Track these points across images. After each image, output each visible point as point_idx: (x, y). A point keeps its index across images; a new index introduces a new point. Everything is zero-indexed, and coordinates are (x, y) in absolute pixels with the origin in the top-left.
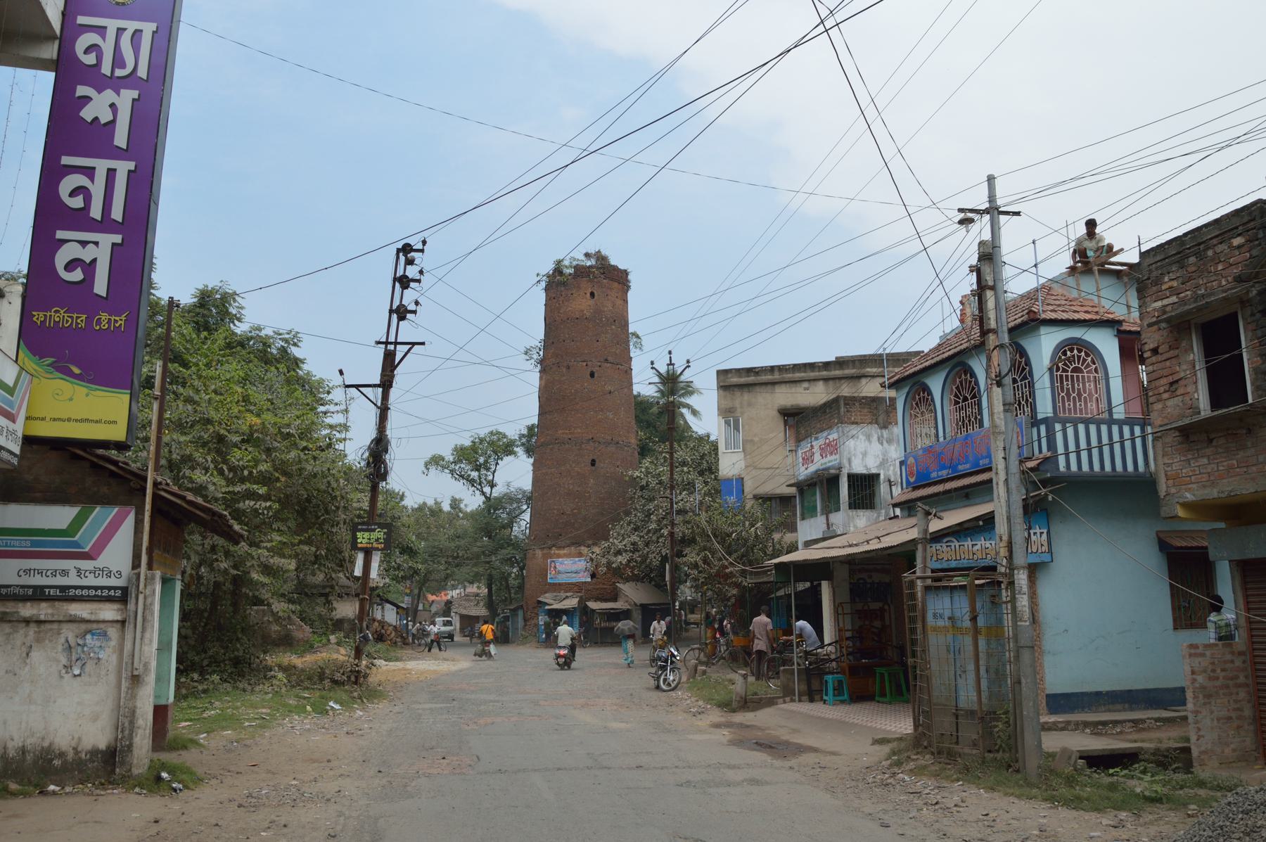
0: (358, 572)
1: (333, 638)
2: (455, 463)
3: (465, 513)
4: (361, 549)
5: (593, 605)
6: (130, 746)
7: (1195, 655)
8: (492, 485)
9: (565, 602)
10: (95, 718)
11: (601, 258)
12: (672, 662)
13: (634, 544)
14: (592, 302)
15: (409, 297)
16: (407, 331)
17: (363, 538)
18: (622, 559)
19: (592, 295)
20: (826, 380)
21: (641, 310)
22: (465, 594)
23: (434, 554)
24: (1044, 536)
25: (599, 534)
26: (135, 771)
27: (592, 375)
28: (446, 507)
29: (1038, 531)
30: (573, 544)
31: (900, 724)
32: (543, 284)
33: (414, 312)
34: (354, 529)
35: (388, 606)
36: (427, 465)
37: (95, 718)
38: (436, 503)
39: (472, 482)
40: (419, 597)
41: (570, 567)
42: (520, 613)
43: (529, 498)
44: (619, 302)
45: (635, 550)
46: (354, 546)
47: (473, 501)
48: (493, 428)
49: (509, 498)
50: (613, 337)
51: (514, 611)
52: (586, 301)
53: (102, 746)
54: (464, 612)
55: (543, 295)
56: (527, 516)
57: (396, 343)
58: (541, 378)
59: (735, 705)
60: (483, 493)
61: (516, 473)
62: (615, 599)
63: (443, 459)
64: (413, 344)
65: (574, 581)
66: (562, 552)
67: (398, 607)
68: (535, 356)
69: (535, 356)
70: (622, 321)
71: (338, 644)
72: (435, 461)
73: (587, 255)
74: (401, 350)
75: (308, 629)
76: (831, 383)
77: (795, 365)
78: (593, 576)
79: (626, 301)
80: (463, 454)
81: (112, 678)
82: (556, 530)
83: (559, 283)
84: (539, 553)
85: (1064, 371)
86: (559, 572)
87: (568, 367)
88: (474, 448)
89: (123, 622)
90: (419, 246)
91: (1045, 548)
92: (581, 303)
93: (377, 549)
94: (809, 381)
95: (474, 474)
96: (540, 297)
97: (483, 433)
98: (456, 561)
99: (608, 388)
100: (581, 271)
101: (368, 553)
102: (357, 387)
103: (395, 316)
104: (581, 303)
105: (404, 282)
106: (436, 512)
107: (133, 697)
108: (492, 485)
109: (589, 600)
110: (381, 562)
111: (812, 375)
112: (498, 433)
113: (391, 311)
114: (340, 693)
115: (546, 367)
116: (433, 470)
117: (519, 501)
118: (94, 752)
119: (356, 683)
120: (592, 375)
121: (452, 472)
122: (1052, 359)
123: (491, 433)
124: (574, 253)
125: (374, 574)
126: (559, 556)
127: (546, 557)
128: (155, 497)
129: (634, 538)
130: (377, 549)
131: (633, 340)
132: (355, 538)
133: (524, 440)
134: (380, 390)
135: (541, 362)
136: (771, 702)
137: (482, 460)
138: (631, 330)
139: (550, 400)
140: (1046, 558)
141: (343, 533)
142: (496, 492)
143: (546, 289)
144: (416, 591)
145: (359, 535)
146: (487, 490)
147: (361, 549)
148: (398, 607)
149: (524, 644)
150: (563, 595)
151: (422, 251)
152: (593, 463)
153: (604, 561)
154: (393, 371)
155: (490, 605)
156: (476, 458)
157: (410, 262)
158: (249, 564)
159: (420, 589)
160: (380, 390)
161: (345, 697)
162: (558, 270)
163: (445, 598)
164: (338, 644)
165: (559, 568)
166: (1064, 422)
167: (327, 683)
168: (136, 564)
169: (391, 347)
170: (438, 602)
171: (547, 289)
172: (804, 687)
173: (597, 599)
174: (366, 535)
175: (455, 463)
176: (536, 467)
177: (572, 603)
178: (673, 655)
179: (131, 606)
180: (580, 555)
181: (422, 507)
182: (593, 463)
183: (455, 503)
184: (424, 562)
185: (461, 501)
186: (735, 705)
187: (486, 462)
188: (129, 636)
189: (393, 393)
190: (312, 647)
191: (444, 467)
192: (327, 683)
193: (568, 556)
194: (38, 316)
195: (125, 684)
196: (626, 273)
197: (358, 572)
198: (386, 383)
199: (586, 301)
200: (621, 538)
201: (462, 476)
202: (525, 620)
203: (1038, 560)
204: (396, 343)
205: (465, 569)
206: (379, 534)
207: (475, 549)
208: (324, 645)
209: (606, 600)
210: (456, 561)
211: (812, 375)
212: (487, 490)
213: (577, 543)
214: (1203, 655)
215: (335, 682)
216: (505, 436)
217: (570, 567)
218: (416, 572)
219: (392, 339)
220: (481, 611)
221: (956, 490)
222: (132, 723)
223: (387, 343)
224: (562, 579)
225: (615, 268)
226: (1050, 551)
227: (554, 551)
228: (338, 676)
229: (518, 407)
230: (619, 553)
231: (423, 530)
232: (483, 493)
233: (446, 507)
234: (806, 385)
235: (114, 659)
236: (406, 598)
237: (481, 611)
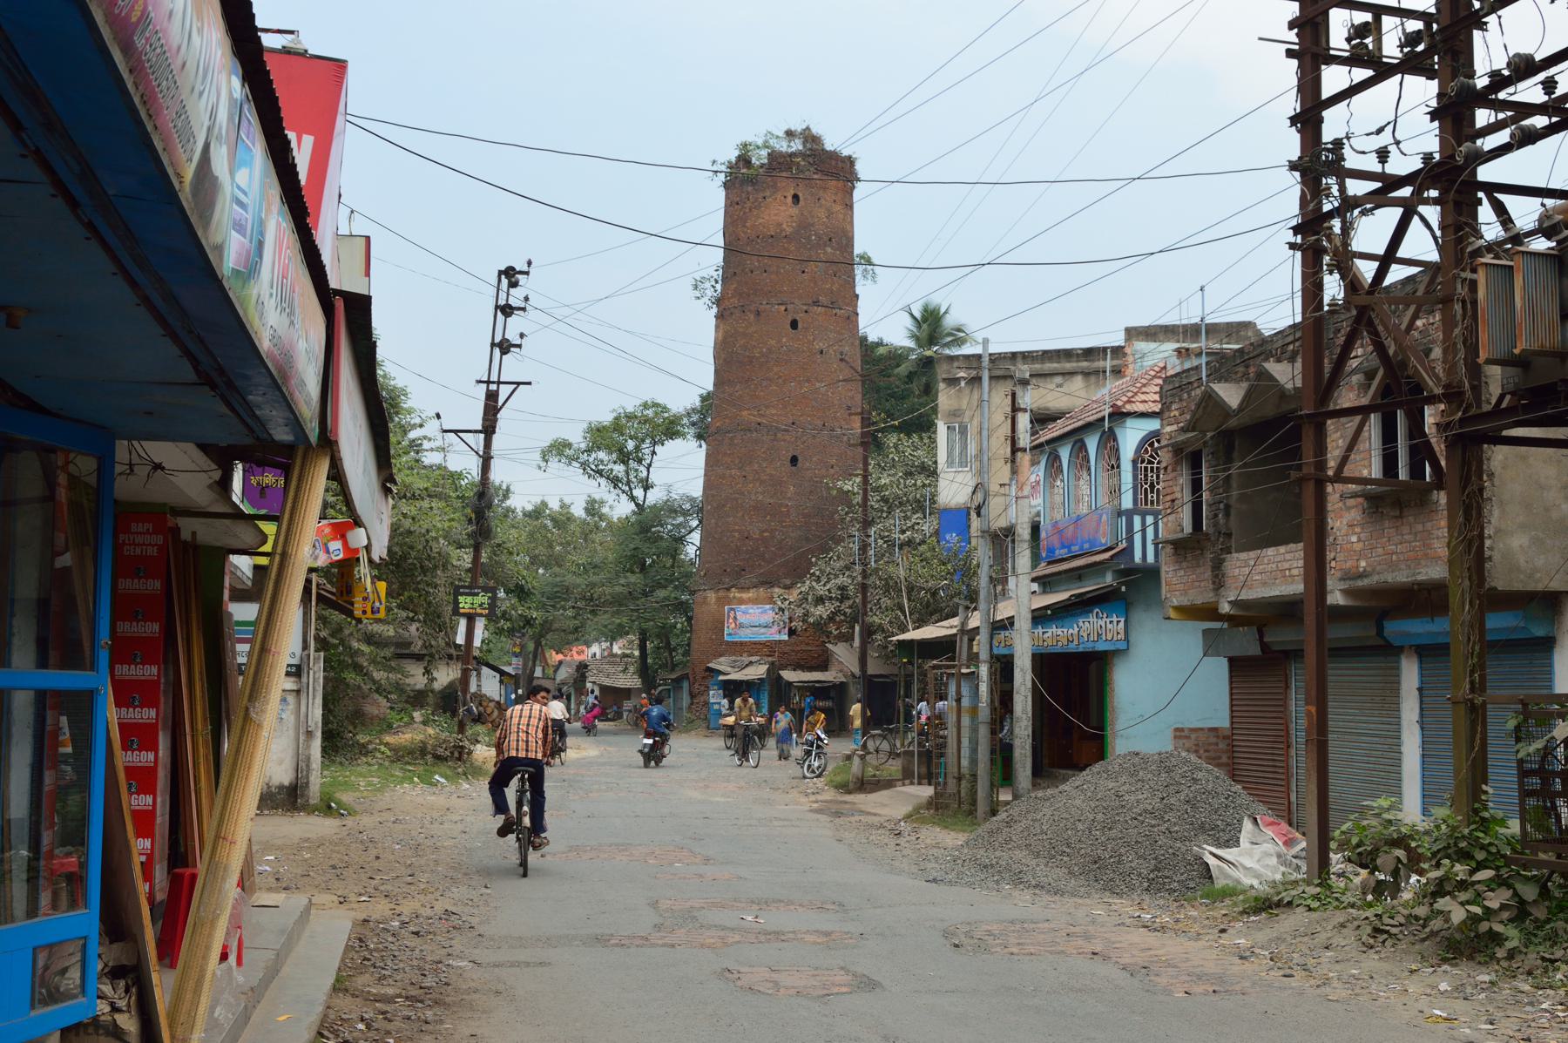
0: (460, 639)
1: (417, 715)
2: (589, 451)
3: (610, 525)
4: (464, 615)
5: (789, 675)
6: (307, 783)
7: (1181, 737)
8: (647, 486)
9: (746, 671)
10: (281, 762)
11: (810, 138)
12: (818, 747)
13: (843, 588)
14: (794, 211)
15: (515, 326)
16: (512, 367)
17: (465, 603)
18: (821, 611)
19: (796, 198)
20: (1086, 374)
21: (873, 223)
22: (605, 656)
23: (559, 595)
24: (1122, 625)
25: (798, 571)
26: (312, 802)
27: (794, 324)
28: (578, 511)
29: (1115, 619)
30: (763, 583)
31: (927, 791)
32: (722, 177)
33: (519, 346)
34: (457, 592)
35: (485, 670)
36: (545, 455)
37: (281, 762)
38: (563, 506)
39: (615, 481)
40: (537, 655)
41: (755, 618)
42: (685, 685)
43: (700, 510)
44: (837, 208)
45: (843, 598)
46: (456, 611)
47: (620, 508)
48: (648, 397)
49: (670, 508)
50: (836, 261)
51: (678, 681)
52: (787, 209)
53: (286, 783)
54: (607, 682)
55: (722, 193)
56: (695, 537)
57: (499, 383)
58: (717, 327)
59: (851, 786)
60: (633, 498)
61: (680, 470)
62: (824, 666)
63: (569, 445)
64: (519, 384)
65: (763, 638)
66: (745, 596)
67: (502, 673)
68: (710, 292)
69: (710, 292)
70: (843, 238)
71: (425, 723)
72: (558, 449)
73: (790, 134)
74: (504, 391)
75: (383, 702)
76: (1093, 379)
77: (1045, 352)
78: (792, 632)
79: (849, 206)
80: (601, 436)
81: (291, 733)
82: (741, 565)
83: (747, 179)
84: (712, 596)
85: (1150, 462)
86: (741, 626)
87: (758, 313)
88: (617, 426)
89: (298, 692)
90: (525, 268)
91: (1121, 636)
92: (778, 213)
93: (481, 615)
94: (1063, 374)
95: (619, 469)
96: (715, 198)
97: (631, 406)
98: (593, 604)
99: (819, 345)
100: (779, 162)
101: (471, 618)
102: (456, 432)
103: (497, 351)
104: (778, 213)
105: (507, 310)
106: (563, 520)
107: (308, 747)
108: (647, 486)
109: (784, 668)
110: (486, 628)
111: (1069, 366)
112: (656, 405)
113: (493, 345)
114: (443, 768)
115: (725, 310)
116: (554, 464)
117: (685, 513)
118: (281, 787)
119: (459, 759)
120: (794, 324)
121: (584, 465)
122: (1138, 451)
123: (645, 406)
124: (765, 124)
125: (477, 643)
126: (741, 602)
127: (722, 602)
128: (318, 595)
129: (841, 580)
130: (481, 615)
131: (858, 270)
132: (456, 603)
133: (695, 418)
134: (482, 436)
135: (718, 302)
136: (889, 784)
137: (631, 445)
138: (857, 250)
139: (732, 359)
140: (1122, 646)
141: (441, 594)
142: (654, 497)
143: (726, 185)
144: (531, 646)
145: (461, 599)
146: (638, 493)
147: (464, 615)
148: (502, 673)
149: (687, 731)
150: (746, 659)
151: (527, 273)
152: (794, 460)
153: (799, 612)
154: (495, 415)
155: (644, 671)
156: (623, 442)
157: (514, 285)
158: (347, 632)
159: (538, 644)
160: (482, 436)
161: (449, 772)
162: (744, 160)
163: (578, 658)
164: (425, 723)
165: (741, 618)
166: (1143, 515)
167: (429, 757)
168: (305, 647)
169: (493, 387)
170: (569, 665)
171: (727, 185)
172: (924, 770)
173: (797, 666)
174: (469, 599)
175: (589, 451)
176: (711, 462)
177: (758, 671)
178: (819, 738)
179: (304, 679)
180: (771, 600)
181: (537, 513)
182: (794, 460)
183: (592, 507)
184: (542, 606)
185: (602, 502)
186: (851, 786)
187: (637, 448)
188: (303, 702)
189: (497, 440)
190: (390, 726)
191: (571, 459)
192: (429, 757)
193: (755, 601)
194: (253, 481)
195: (302, 738)
196: (850, 161)
197: (460, 639)
198: (489, 429)
199: (787, 209)
200: (830, 578)
201: (600, 473)
202: (692, 696)
203: (1113, 648)
204: (499, 383)
205: (603, 618)
206: (483, 598)
207: (618, 589)
208: (407, 725)
209: (811, 669)
210: (593, 604)
211: (1069, 366)
212: (638, 493)
213: (768, 582)
214: (1187, 737)
215: (438, 757)
216: (665, 409)
217: (755, 618)
218: (528, 622)
219: (494, 378)
220: (630, 681)
221: (1066, 571)
222: (308, 766)
223: (488, 382)
224: (745, 635)
225: (834, 156)
226: (1127, 639)
227: (734, 593)
228: (440, 751)
229: (686, 377)
230: (820, 600)
231: (541, 550)
232: (633, 498)
233: (578, 511)
234: (1058, 380)
235: (292, 718)
236: (514, 660)
237: (630, 681)
